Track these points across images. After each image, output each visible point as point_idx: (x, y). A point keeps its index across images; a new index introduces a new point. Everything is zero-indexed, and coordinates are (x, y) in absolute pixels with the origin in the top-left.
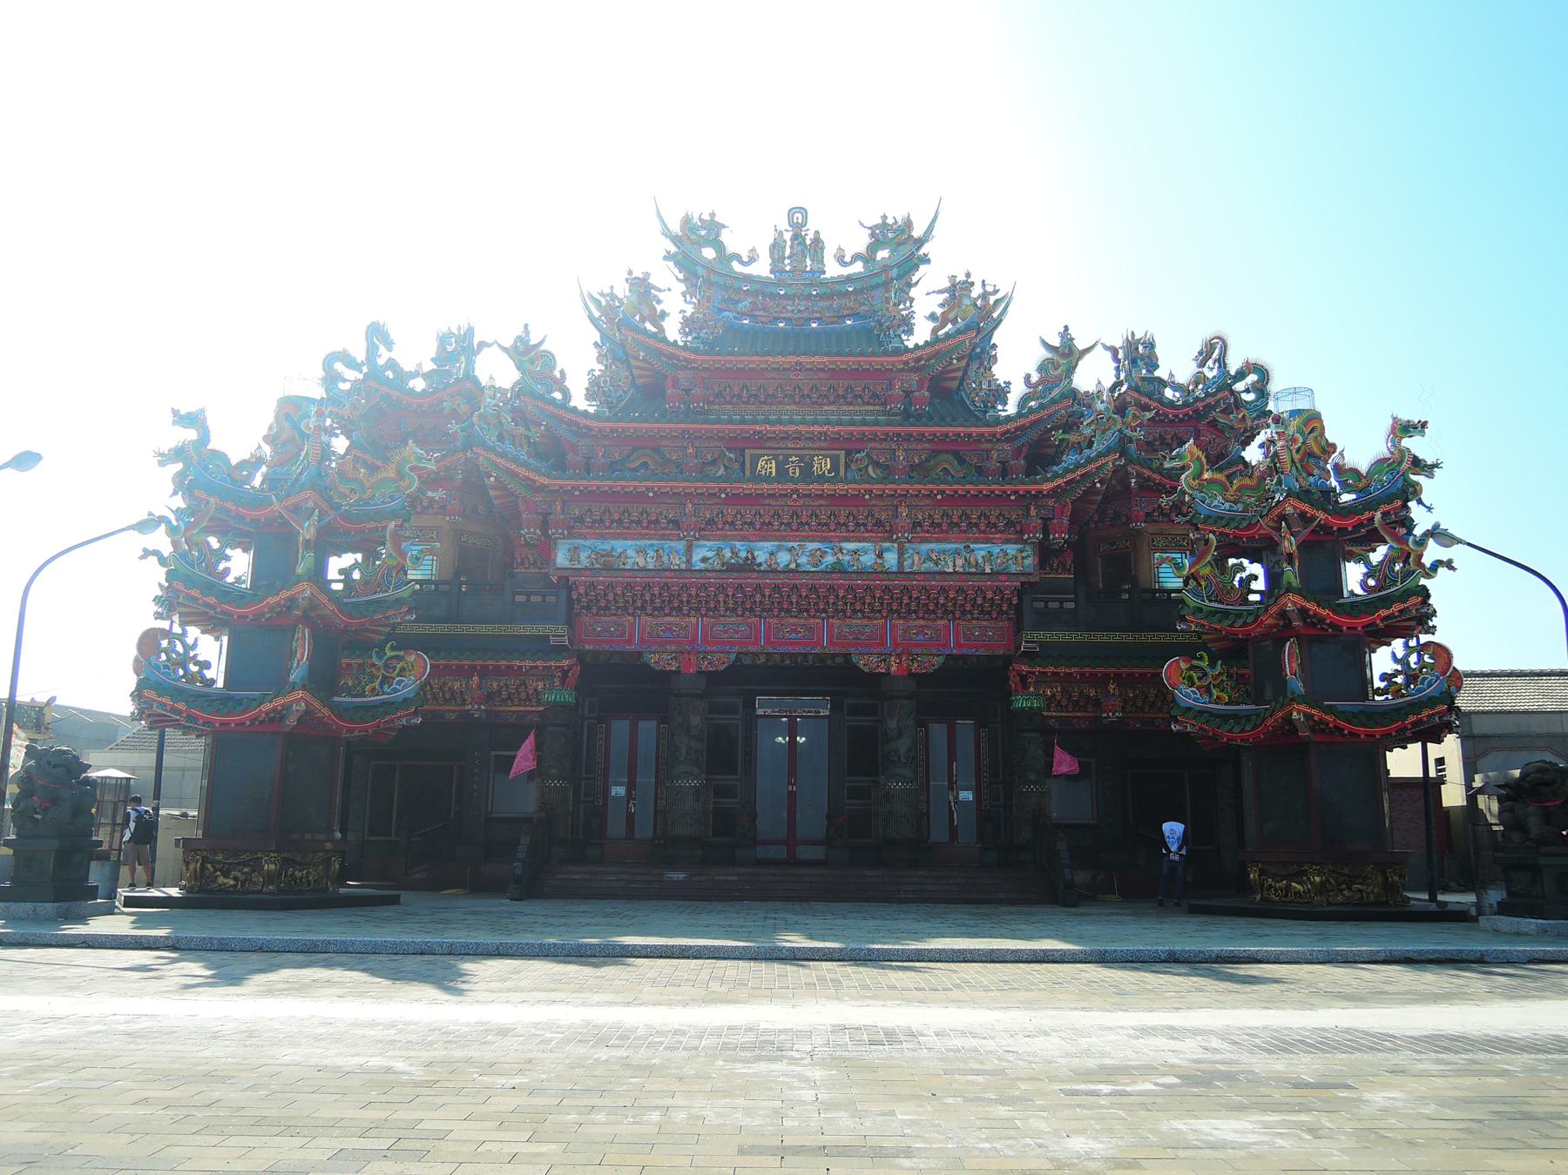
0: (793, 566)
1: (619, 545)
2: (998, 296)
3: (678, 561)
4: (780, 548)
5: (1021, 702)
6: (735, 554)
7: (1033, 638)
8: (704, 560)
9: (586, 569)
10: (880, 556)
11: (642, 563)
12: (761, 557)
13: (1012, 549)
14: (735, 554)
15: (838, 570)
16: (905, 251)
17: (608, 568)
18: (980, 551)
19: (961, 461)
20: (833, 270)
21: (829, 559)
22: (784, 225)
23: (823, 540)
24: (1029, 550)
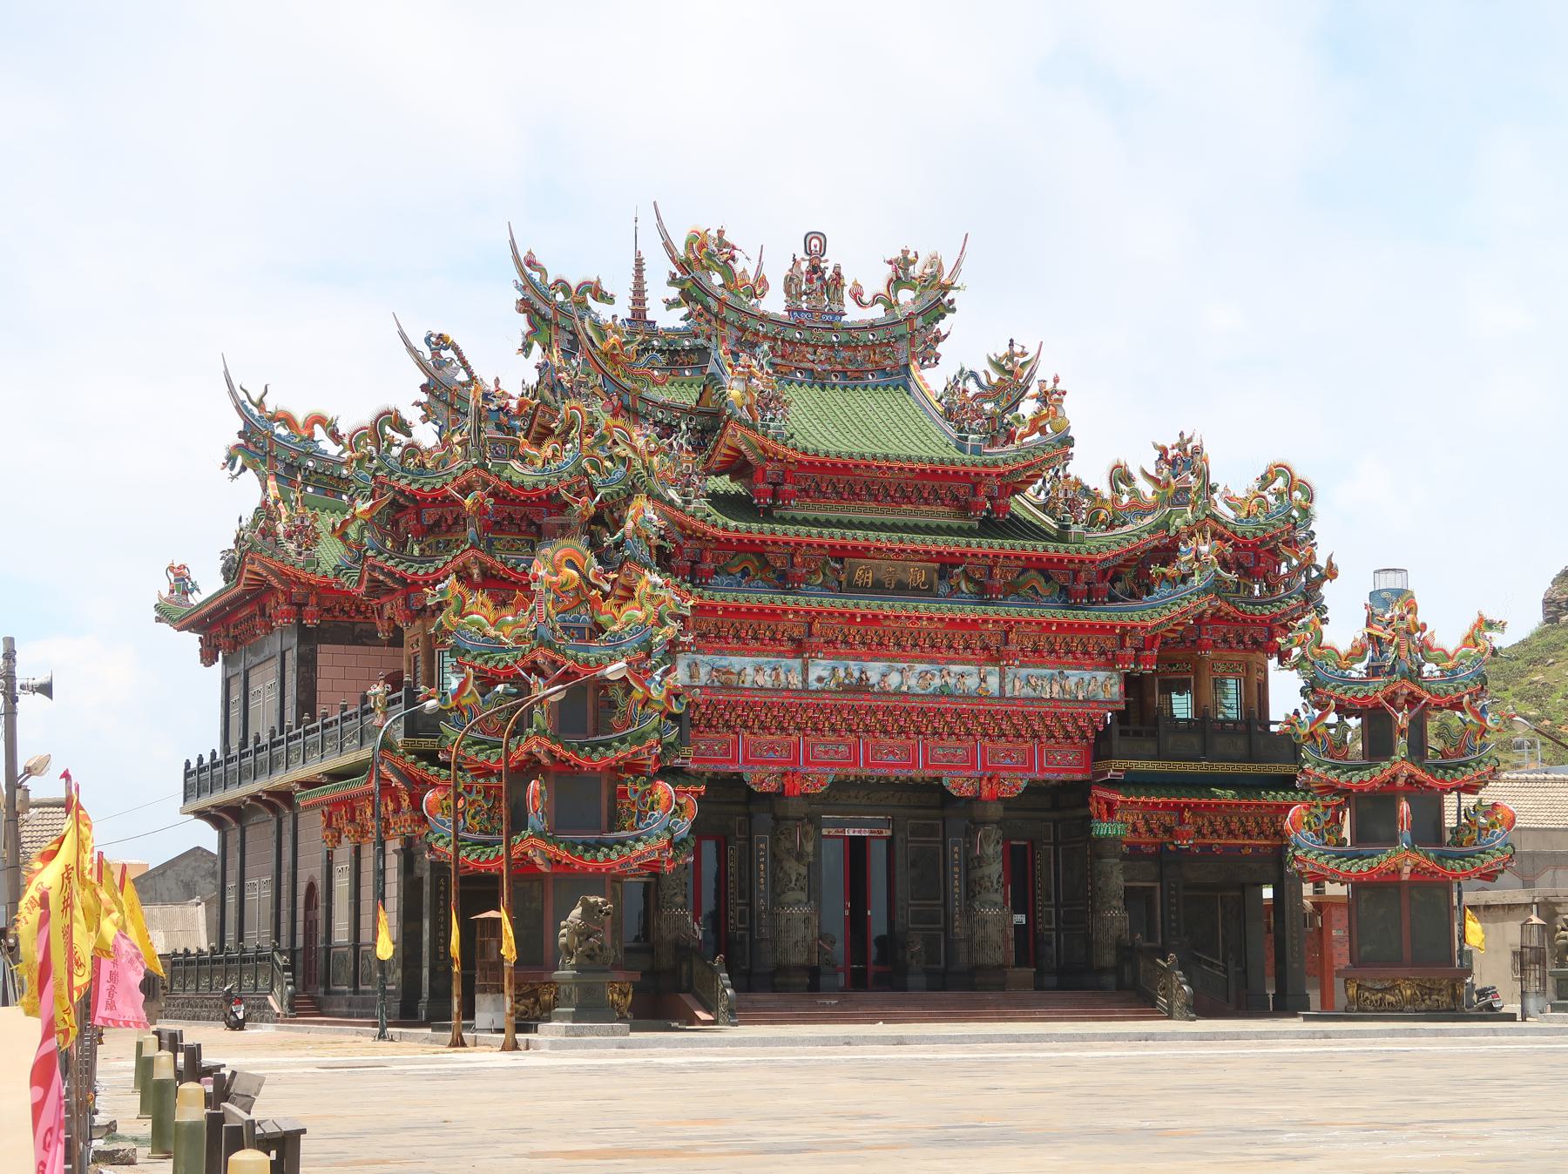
0: (904, 688)
1: (736, 662)
2: (1026, 359)
3: (796, 681)
4: (891, 669)
5: (1103, 829)
6: (848, 675)
7: (1115, 768)
8: (820, 679)
9: (706, 686)
10: (983, 680)
11: (760, 680)
12: (874, 678)
13: (1101, 675)
14: (848, 675)
15: (943, 693)
16: (932, 294)
17: (726, 686)
18: (1074, 676)
19: (1048, 579)
20: (853, 314)
21: (937, 682)
22: (801, 254)
23: (932, 661)
24: (1116, 678)
